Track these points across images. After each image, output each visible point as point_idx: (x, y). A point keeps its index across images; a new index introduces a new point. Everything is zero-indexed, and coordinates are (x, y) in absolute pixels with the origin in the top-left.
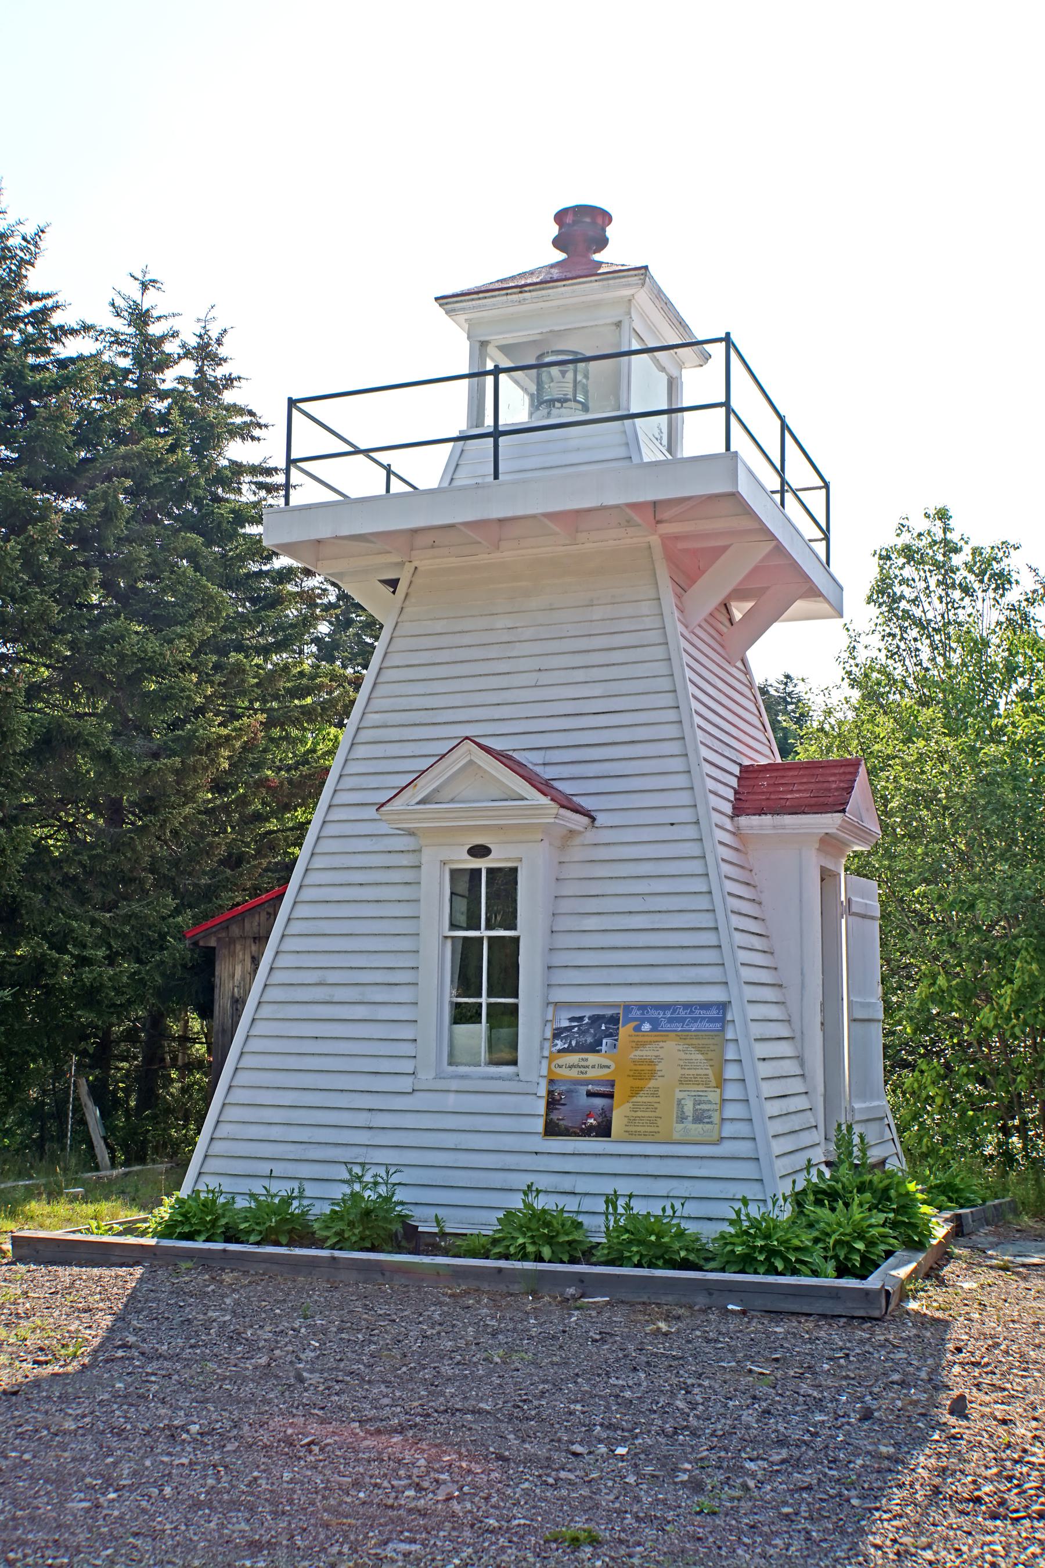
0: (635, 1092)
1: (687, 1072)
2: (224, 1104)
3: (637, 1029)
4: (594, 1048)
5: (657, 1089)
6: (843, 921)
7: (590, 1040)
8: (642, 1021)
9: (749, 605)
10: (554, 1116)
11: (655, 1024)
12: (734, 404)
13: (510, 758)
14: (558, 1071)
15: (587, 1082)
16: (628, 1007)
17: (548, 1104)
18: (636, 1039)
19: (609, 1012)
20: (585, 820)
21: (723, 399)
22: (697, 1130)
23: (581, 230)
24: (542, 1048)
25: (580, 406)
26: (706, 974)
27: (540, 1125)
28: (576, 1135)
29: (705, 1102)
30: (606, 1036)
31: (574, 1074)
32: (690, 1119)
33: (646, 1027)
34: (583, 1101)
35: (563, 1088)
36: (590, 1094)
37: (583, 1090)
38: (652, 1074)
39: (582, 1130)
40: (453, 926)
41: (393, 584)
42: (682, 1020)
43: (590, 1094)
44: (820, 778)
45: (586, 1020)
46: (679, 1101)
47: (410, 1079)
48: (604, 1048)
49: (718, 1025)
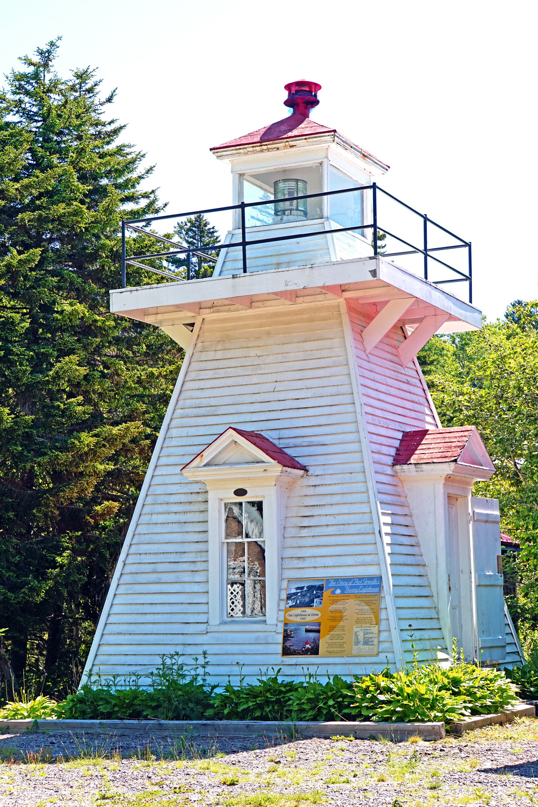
0: (332, 628)
1: (360, 616)
2: (99, 645)
3: (333, 592)
4: (309, 605)
5: (343, 627)
6: (471, 526)
7: (307, 600)
8: (336, 588)
9: (416, 325)
10: (288, 644)
11: (343, 589)
12: (379, 224)
13: (259, 436)
14: (290, 618)
15: (305, 624)
16: (328, 580)
17: (284, 637)
18: (332, 598)
19: (317, 584)
20: (302, 472)
21: (372, 223)
22: (366, 648)
23: (302, 97)
24: (279, 605)
25: (302, 213)
26: (368, 559)
27: (280, 651)
28: (300, 654)
29: (370, 633)
30: (316, 598)
31: (298, 619)
32: (362, 643)
33: (338, 591)
34: (303, 634)
35: (292, 628)
36: (307, 631)
37: (303, 628)
38: (341, 619)
39: (303, 651)
40: (228, 536)
41: (192, 325)
42: (358, 587)
43: (307, 631)
44: (447, 440)
45: (305, 589)
46: (356, 633)
47: (205, 626)
48: (315, 604)
49: (377, 589)
